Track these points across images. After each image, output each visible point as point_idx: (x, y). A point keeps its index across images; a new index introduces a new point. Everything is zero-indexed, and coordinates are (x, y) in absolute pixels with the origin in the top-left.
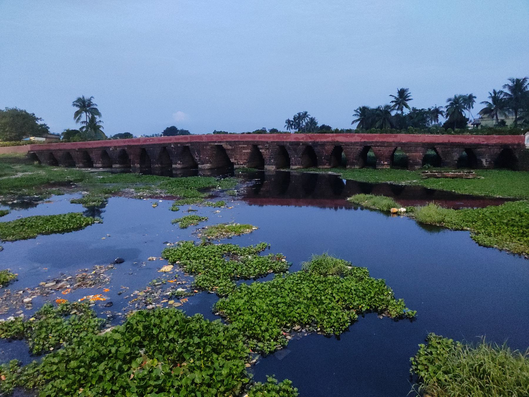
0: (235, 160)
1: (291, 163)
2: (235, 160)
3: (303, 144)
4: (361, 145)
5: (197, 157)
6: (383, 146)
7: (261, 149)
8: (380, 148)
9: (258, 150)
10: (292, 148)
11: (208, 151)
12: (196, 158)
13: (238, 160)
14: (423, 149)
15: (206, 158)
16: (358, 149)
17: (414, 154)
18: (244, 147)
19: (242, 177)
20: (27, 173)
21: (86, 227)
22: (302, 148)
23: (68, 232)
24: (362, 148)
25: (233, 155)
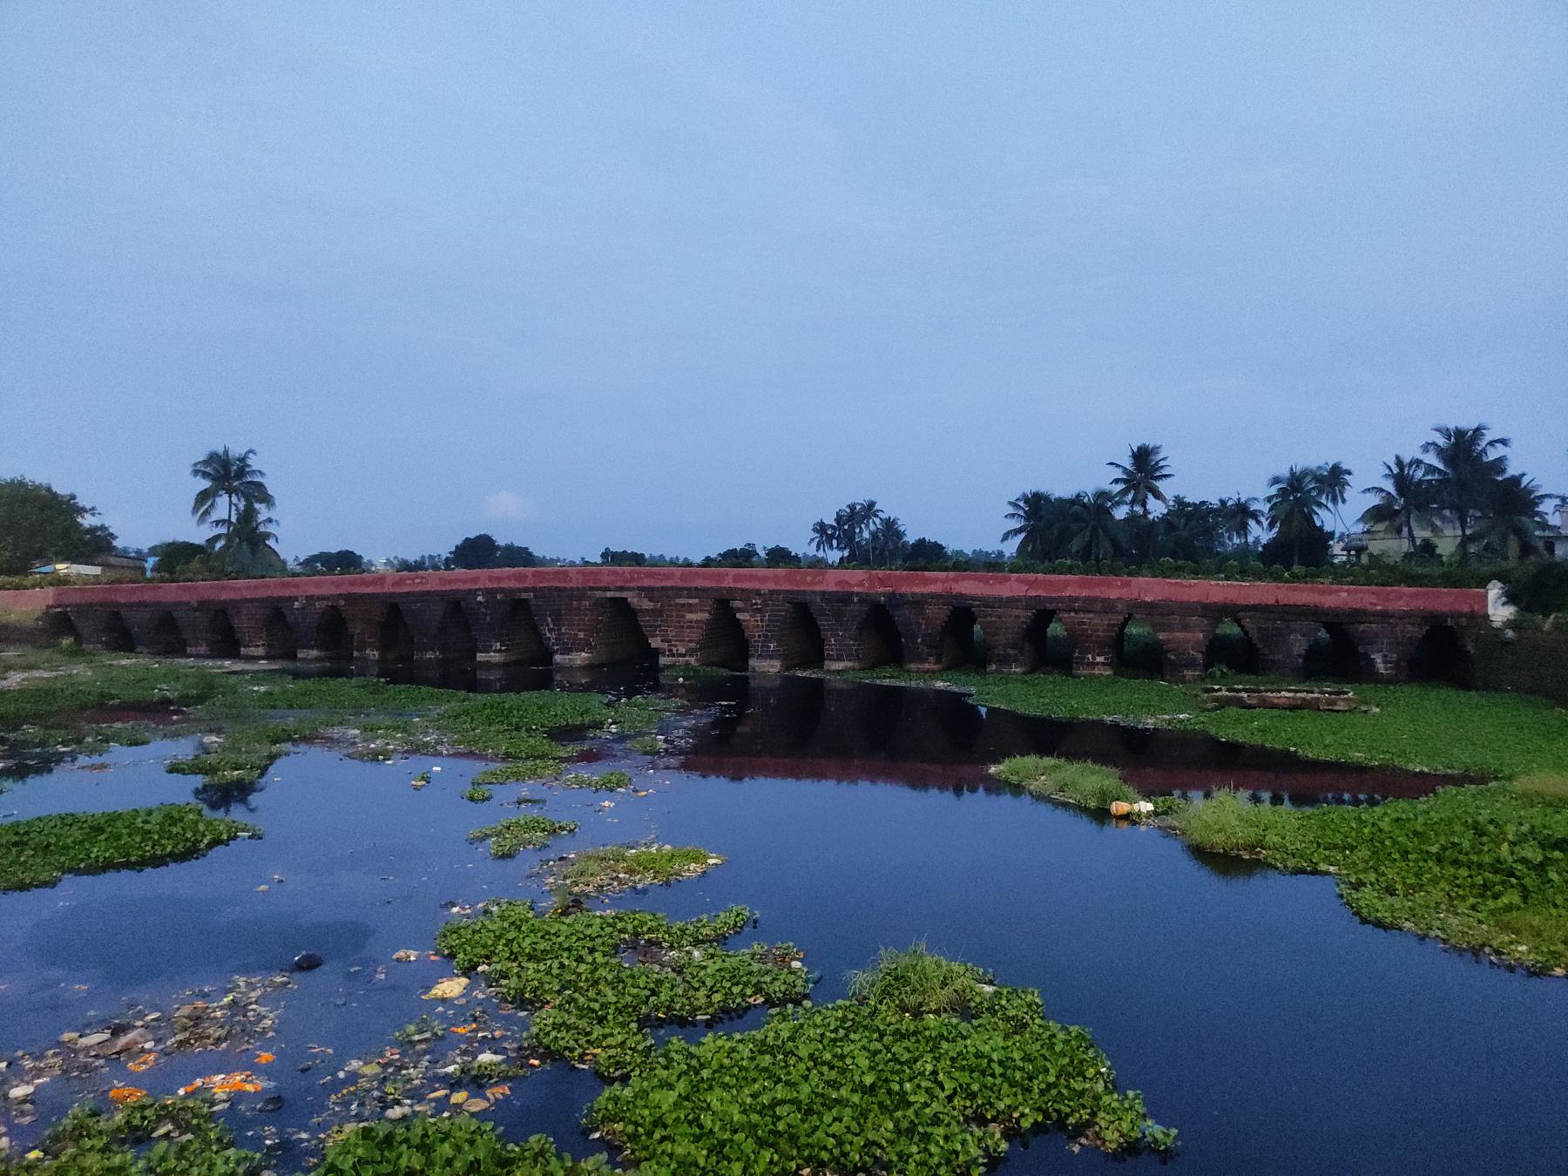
2: (662, 641)
12: (548, 635)
13: (669, 641)
18: (690, 605)
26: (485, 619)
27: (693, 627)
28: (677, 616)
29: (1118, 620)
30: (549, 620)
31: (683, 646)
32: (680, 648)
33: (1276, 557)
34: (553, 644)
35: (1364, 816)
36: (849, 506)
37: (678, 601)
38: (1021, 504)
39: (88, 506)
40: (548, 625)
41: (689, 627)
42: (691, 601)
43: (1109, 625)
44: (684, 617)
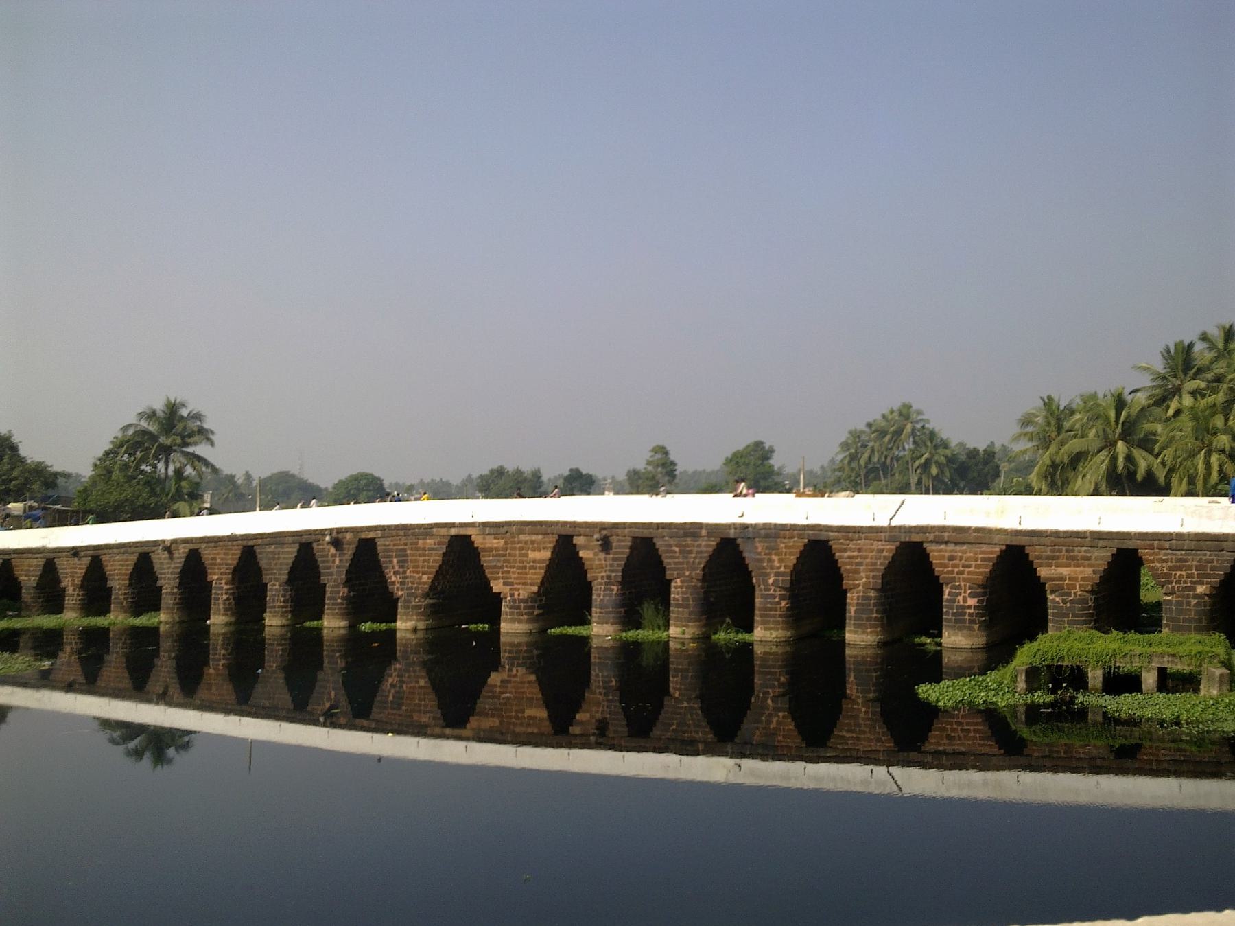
0: (505, 584)
1: (672, 596)
2: (505, 584)
3: (709, 535)
4: (889, 540)
5: (396, 573)
6: (964, 543)
7: (585, 547)
8: (951, 547)
9: (574, 550)
10: (676, 546)
11: (430, 555)
12: (393, 579)
13: (512, 584)
14: (1081, 403)
15: (420, 578)
16: (882, 551)
17: (1064, 571)
18: (533, 542)
19: (594, 567)
20: (88, 552)
21: (537, 475)
22: (707, 546)
23: (454, 524)
24: (893, 547)
25: (501, 567)
26: (334, 562)
27: (535, 568)
28: (521, 555)
29: (992, 553)
30: (395, 561)
31: (524, 589)
32: (521, 592)
33: (775, 529)
34: (398, 589)
35: (145, 492)
36: (170, 761)
37: (522, 537)
38: (283, 642)
39: (50, 465)
40: (393, 567)
41: (532, 568)
42: (534, 537)
43: (983, 559)
44: (527, 555)
